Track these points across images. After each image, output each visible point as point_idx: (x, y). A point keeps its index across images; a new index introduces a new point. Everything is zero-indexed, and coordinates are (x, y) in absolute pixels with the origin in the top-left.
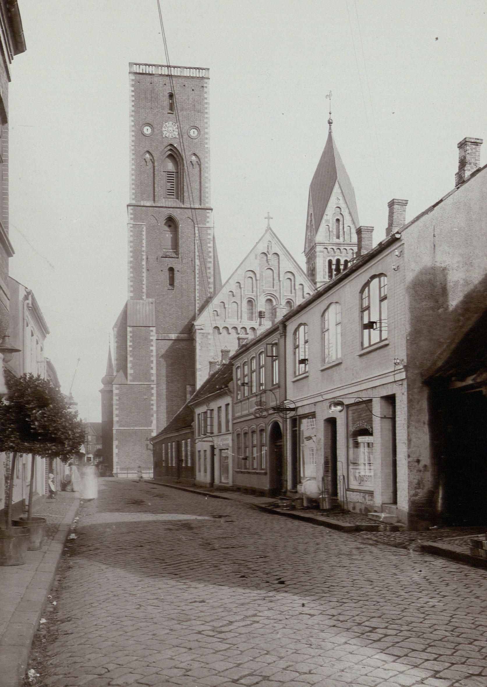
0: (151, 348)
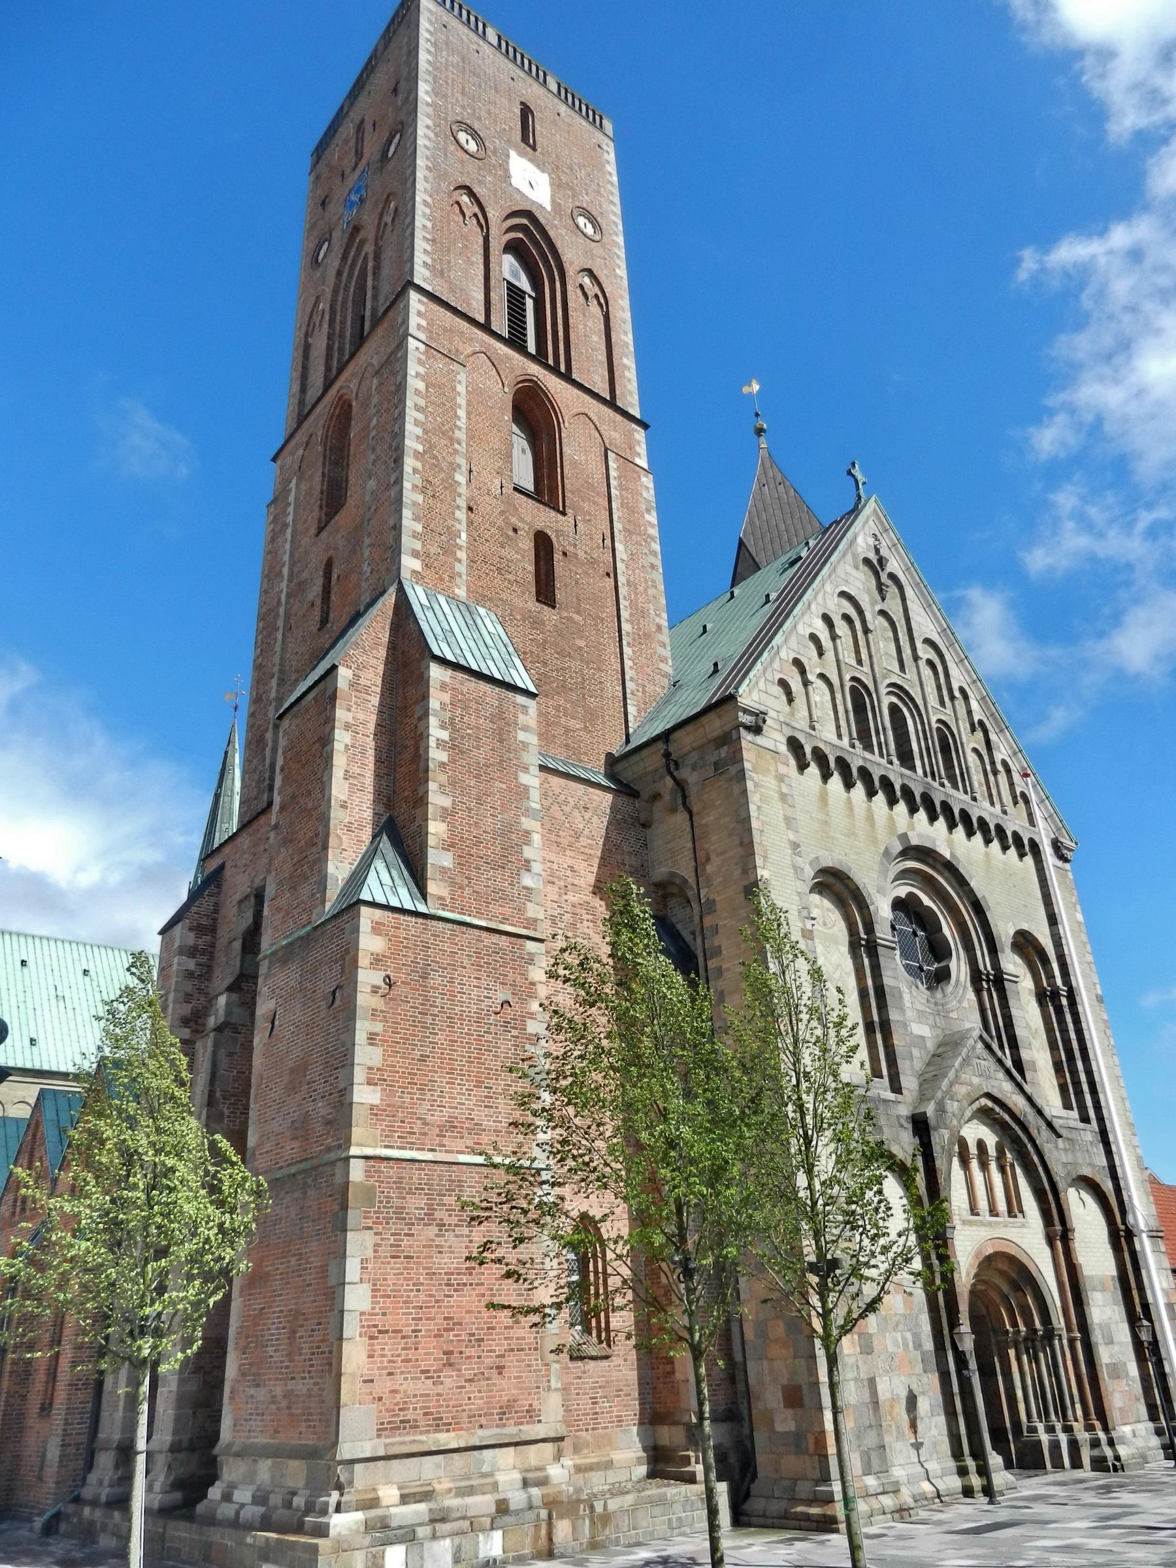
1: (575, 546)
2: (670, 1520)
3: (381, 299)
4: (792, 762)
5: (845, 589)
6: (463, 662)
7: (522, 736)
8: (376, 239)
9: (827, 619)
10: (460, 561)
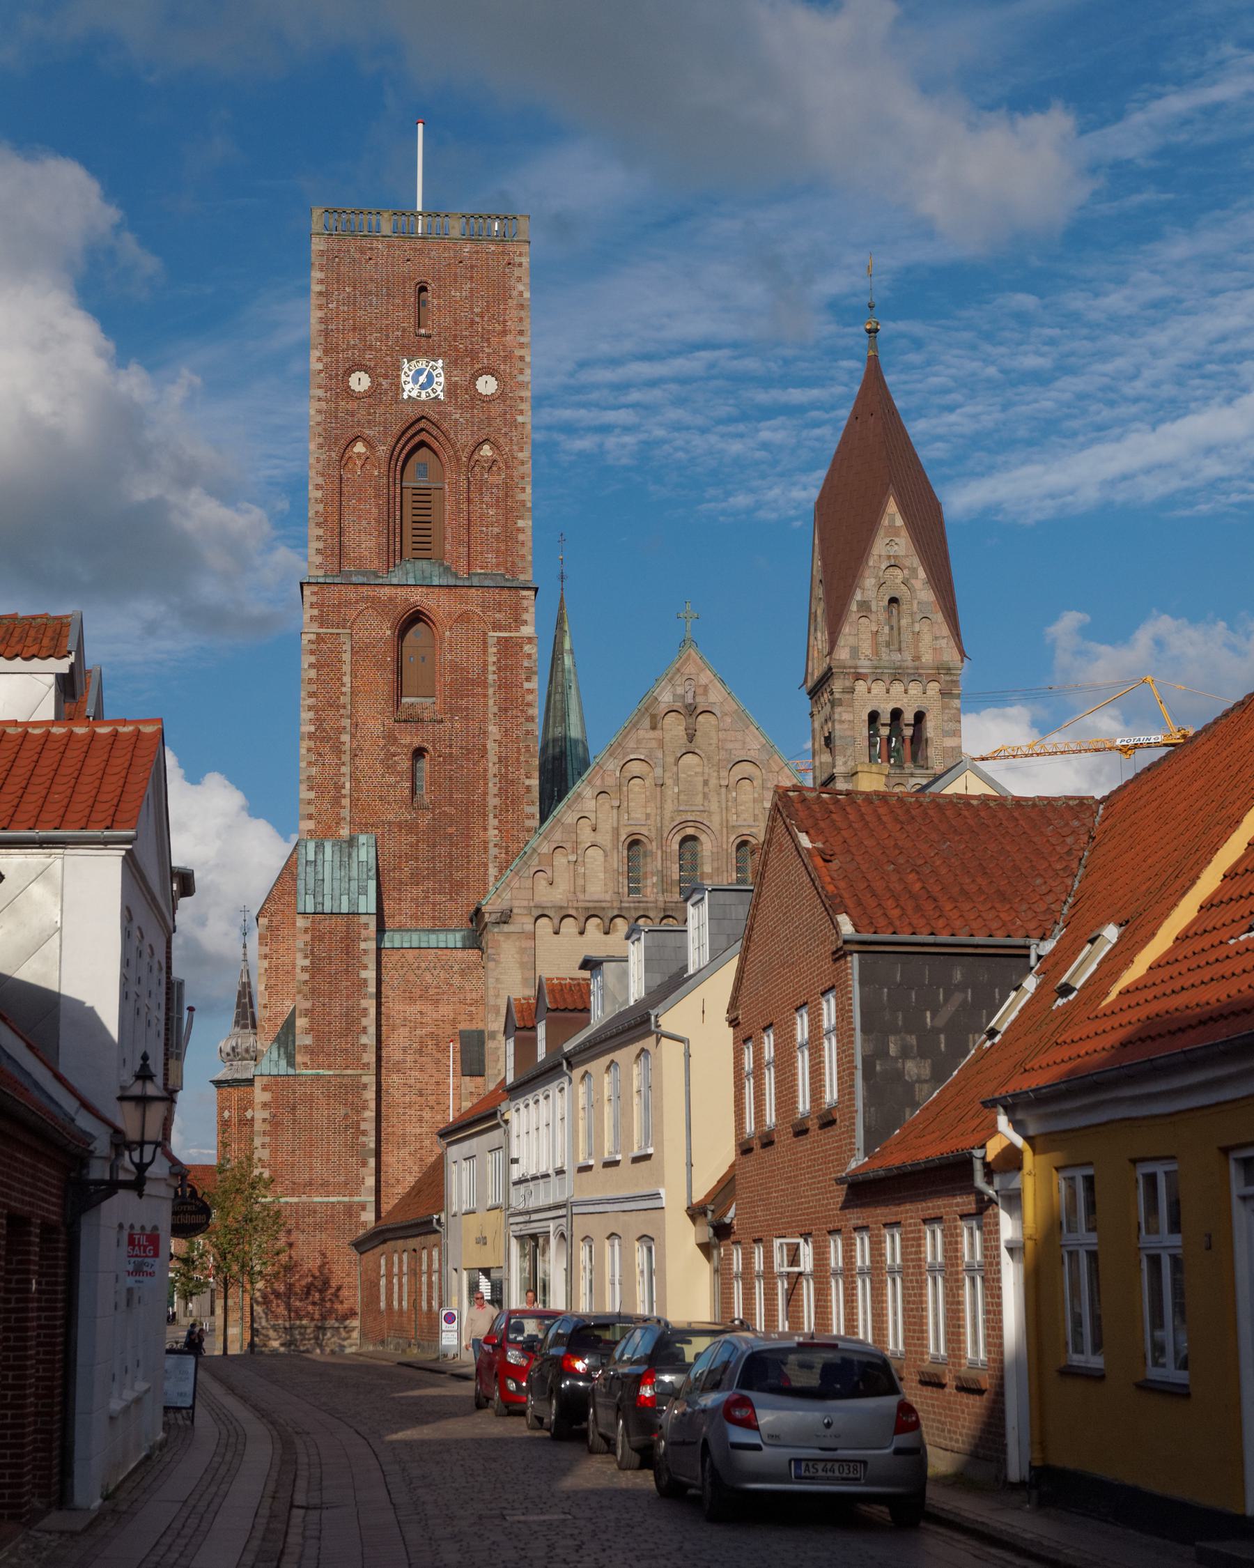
0: (364, 974)
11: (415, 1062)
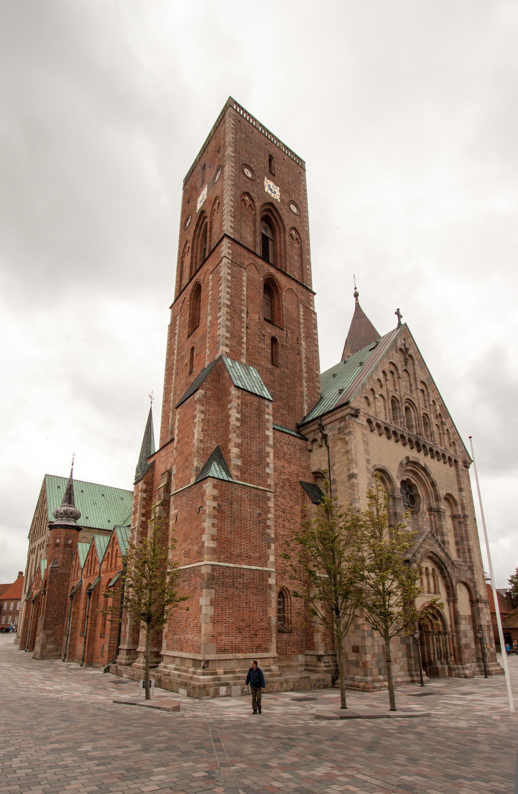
1: (286, 342)
2: (311, 684)
3: (213, 241)
4: (369, 429)
5: (392, 361)
6: (246, 388)
7: (267, 417)
8: (211, 216)
9: (384, 372)
10: (243, 349)
11: (281, 493)
